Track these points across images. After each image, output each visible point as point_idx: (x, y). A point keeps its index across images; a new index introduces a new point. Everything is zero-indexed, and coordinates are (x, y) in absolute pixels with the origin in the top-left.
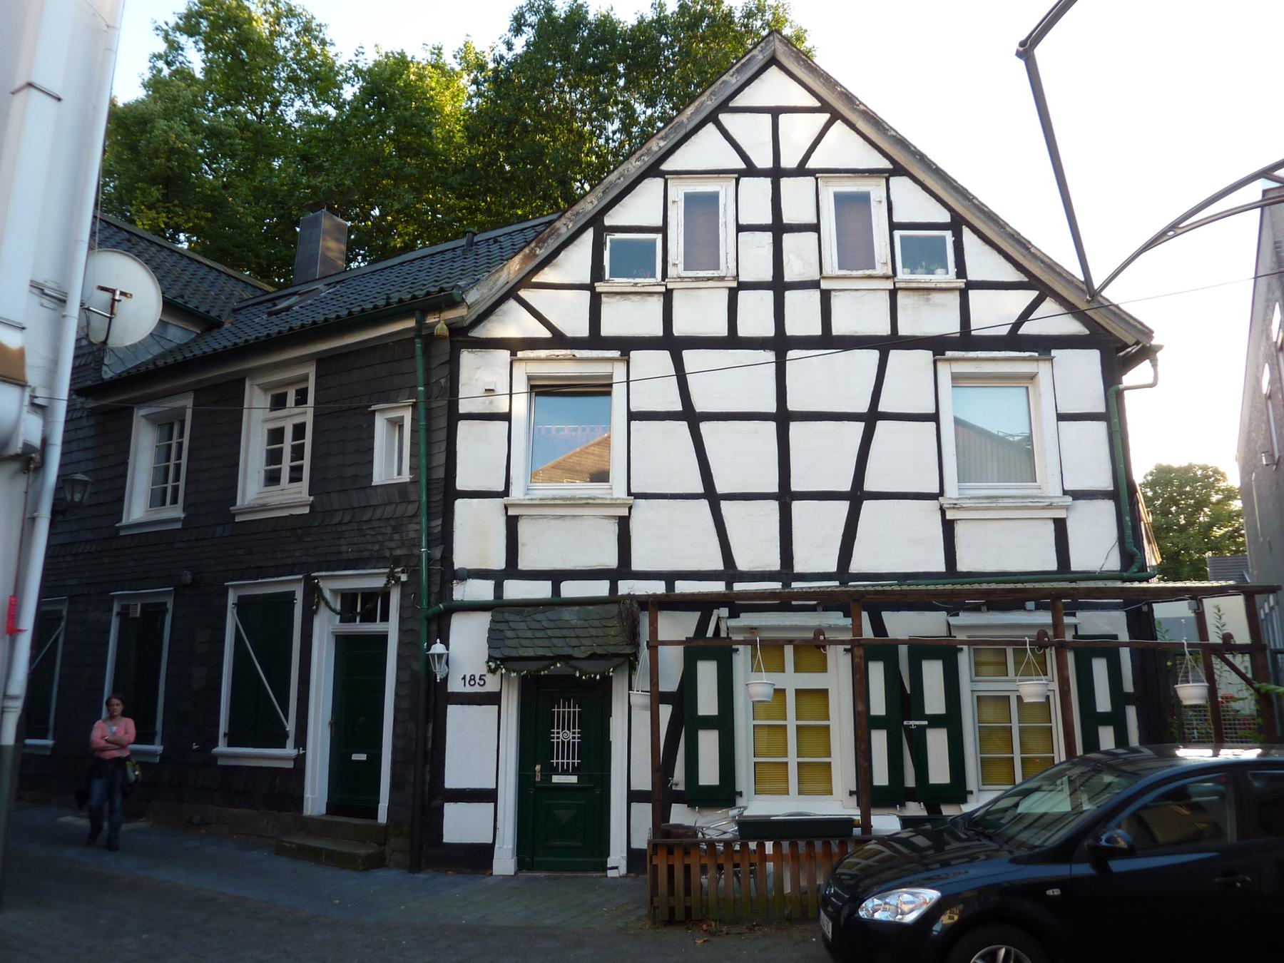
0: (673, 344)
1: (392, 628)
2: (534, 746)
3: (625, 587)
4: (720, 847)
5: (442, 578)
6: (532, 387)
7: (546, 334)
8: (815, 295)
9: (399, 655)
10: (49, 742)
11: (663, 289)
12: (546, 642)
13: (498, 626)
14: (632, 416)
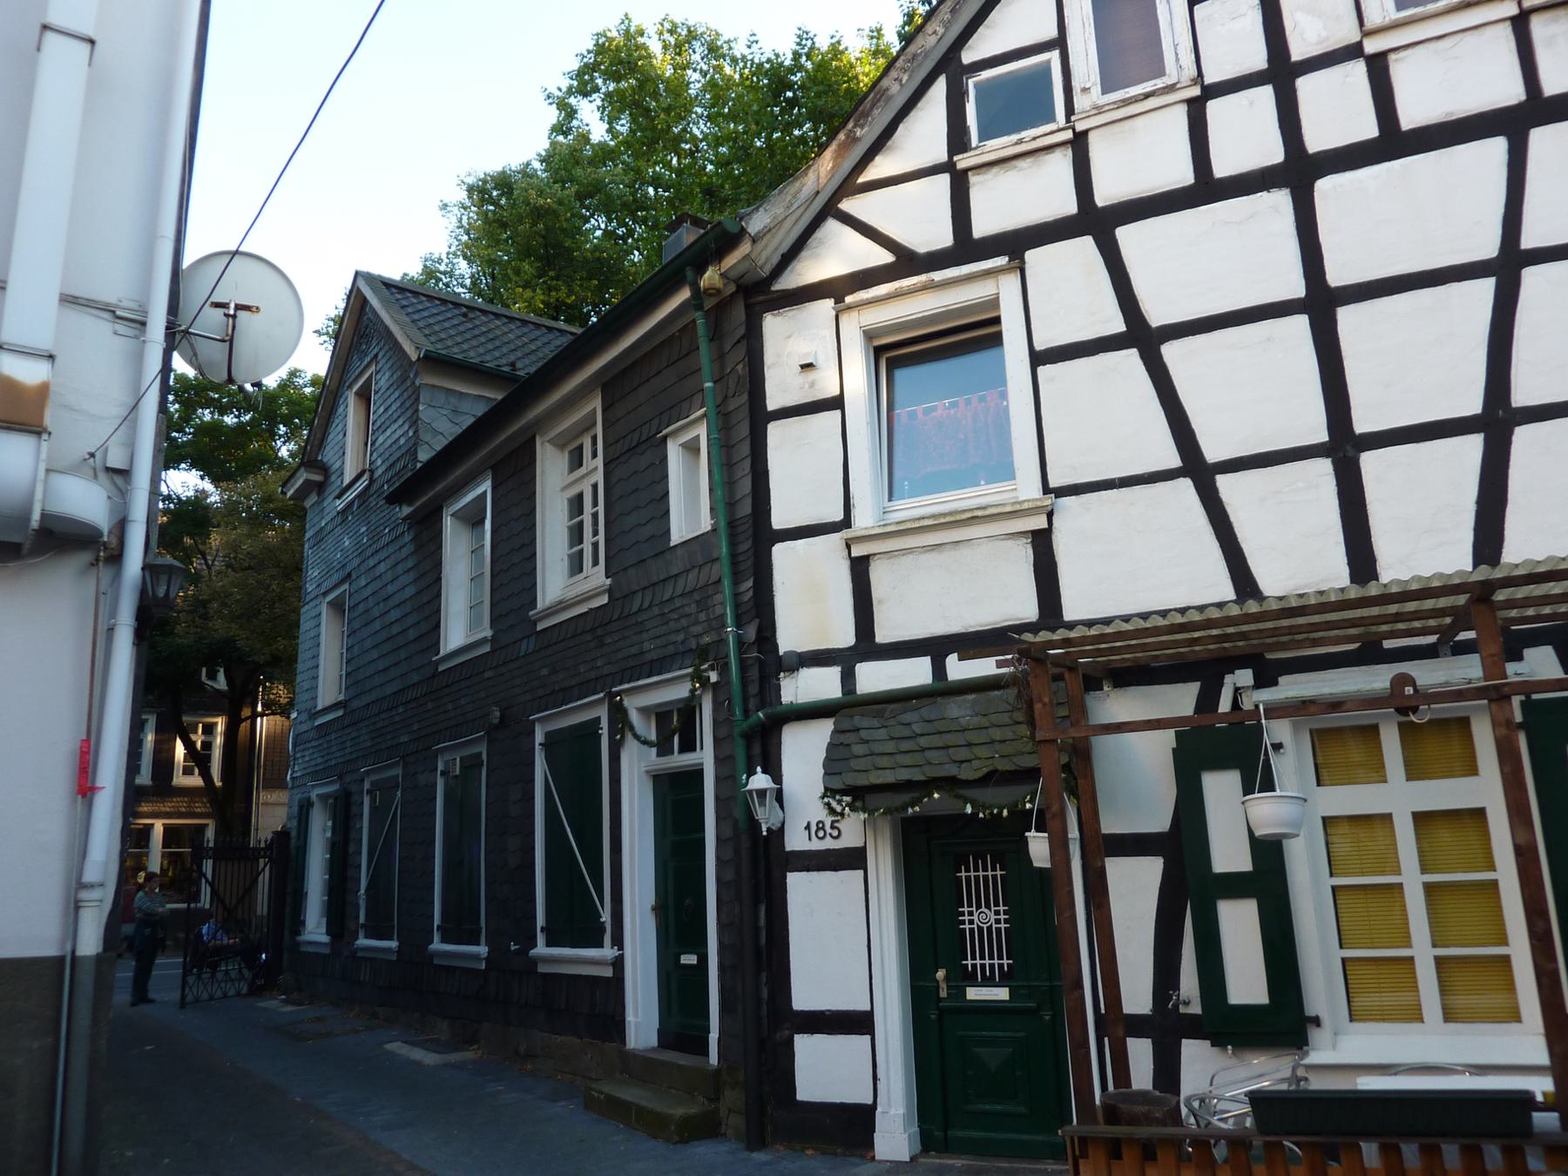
0: (1096, 222)
1: (705, 756)
2: (930, 940)
4: (1220, 1152)
5: (761, 670)
6: (879, 351)
7: (886, 257)
8: (1357, 71)
10: (394, 944)
11: (1069, 135)
13: (844, 738)
14: (1039, 358)
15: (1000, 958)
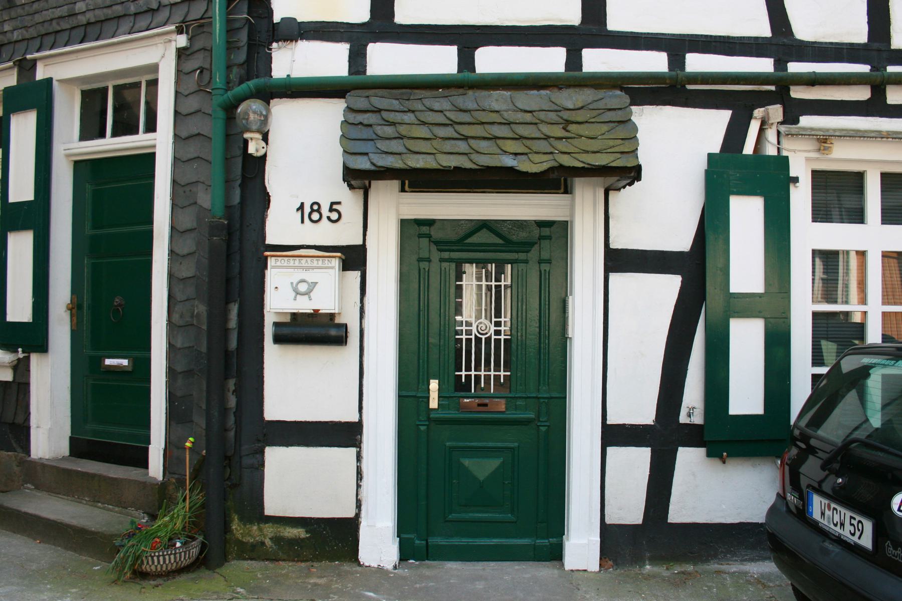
1: (162, 142)
3: (596, 60)
9: (174, 182)
12: (462, 146)
15: (497, 368)
